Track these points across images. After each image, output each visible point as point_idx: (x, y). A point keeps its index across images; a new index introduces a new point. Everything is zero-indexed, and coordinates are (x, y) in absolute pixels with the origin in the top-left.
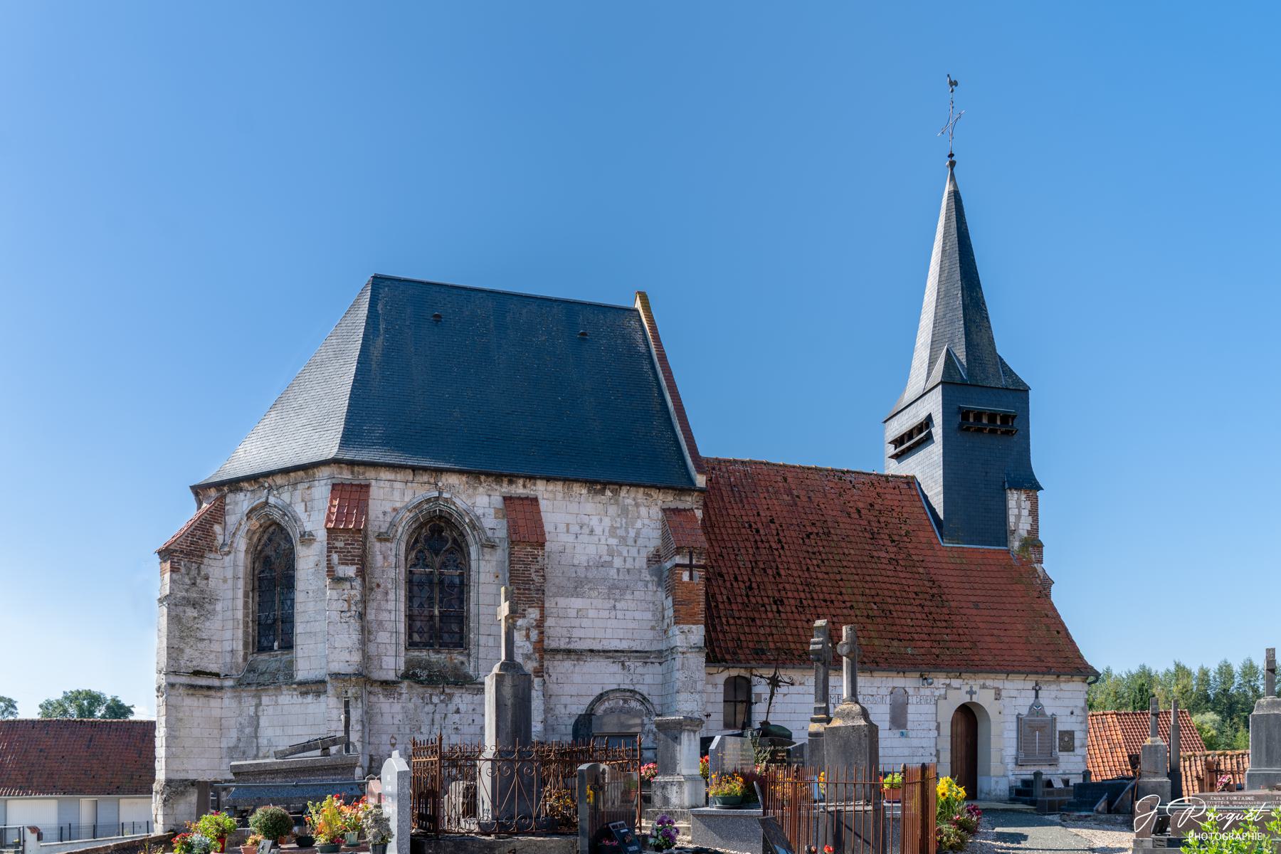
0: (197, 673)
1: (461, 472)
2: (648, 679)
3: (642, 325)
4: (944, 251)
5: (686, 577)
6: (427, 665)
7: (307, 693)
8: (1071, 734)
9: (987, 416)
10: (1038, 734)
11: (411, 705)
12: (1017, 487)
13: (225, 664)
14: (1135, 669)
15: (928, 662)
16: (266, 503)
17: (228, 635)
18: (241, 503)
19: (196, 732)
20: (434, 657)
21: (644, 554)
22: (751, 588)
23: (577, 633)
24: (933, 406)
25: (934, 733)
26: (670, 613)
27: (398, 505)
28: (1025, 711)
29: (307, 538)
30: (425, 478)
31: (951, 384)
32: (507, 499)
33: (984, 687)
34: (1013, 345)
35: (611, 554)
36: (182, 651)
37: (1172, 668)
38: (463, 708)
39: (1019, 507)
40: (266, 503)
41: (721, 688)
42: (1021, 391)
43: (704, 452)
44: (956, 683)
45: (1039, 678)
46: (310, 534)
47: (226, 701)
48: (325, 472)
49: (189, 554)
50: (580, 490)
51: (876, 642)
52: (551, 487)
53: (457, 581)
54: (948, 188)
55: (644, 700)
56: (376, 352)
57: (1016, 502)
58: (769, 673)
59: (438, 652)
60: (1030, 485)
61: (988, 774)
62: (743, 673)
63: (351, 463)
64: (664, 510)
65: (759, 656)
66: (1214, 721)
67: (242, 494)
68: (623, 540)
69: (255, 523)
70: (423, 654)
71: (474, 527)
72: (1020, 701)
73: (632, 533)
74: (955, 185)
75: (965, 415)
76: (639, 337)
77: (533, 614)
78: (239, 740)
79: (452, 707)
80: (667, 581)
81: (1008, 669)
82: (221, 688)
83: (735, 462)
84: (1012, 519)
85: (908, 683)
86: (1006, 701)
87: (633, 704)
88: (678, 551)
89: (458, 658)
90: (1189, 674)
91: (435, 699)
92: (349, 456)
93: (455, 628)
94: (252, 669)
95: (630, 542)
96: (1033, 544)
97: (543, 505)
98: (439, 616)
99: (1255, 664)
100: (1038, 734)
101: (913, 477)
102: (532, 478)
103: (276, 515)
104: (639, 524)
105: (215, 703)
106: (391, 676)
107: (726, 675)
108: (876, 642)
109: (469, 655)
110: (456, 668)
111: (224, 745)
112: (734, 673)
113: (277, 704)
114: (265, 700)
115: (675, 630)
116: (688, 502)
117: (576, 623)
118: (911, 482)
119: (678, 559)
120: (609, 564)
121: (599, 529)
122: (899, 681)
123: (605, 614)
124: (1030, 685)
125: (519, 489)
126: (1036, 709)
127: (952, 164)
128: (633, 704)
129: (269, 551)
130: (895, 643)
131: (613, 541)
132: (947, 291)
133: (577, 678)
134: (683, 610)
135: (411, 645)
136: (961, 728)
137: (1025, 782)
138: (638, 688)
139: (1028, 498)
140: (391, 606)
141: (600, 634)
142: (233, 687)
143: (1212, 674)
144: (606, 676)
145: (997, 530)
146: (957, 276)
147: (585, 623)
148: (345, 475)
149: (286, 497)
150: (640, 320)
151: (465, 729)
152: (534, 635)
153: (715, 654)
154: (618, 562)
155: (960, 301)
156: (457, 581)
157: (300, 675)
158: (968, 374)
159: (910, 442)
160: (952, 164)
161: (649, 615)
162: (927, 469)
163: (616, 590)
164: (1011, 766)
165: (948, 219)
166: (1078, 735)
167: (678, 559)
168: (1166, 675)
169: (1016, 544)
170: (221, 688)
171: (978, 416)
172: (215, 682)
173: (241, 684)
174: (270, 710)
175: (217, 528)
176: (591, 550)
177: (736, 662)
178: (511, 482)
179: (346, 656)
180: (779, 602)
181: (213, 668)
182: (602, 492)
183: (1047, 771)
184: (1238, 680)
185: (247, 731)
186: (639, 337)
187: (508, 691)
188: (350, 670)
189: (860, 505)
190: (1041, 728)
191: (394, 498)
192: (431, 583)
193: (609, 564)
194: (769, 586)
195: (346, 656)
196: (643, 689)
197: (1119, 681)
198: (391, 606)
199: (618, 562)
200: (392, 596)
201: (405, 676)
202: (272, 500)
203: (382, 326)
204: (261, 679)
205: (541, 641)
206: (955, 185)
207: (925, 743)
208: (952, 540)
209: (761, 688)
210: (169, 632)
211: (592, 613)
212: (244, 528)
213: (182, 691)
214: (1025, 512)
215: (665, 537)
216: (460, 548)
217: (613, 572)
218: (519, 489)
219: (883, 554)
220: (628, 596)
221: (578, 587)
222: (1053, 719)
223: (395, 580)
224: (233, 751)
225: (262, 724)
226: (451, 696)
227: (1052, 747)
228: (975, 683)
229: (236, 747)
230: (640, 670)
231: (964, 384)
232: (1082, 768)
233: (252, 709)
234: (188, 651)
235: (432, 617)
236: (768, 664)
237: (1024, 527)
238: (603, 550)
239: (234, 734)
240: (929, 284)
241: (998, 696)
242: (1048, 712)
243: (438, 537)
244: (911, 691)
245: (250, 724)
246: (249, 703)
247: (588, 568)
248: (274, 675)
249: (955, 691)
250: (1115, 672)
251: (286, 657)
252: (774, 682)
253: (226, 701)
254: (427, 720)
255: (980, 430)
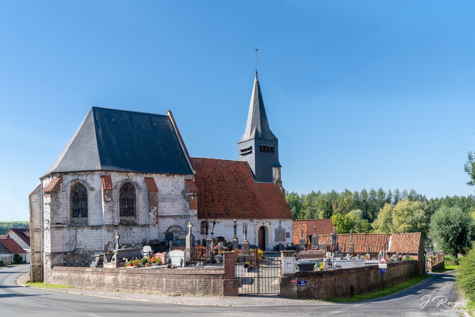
0: (57, 224)
1: (134, 172)
2: (182, 223)
3: (171, 122)
4: (254, 99)
5: (193, 198)
6: (125, 221)
7: (93, 229)
8: (289, 233)
9: (266, 146)
10: (280, 233)
11: (122, 231)
12: (275, 166)
13: (64, 221)
14: (330, 191)
15: (252, 217)
16: (78, 179)
17: (65, 213)
18: (68, 179)
19: (58, 239)
20: (127, 219)
21: (180, 191)
22: (205, 197)
23: (164, 212)
24: (252, 144)
25: (254, 234)
26: (188, 206)
27: (118, 181)
28: (277, 228)
29: (92, 189)
30: (124, 174)
31: (257, 138)
32: (146, 178)
33: (266, 222)
34: (275, 127)
35: (172, 191)
36: (54, 218)
37: (344, 191)
38: (135, 231)
39: (276, 172)
40: (78, 179)
41: (200, 224)
42: (276, 141)
43: (191, 156)
44: (259, 221)
45: (281, 219)
46: (93, 188)
47: (65, 231)
48: (98, 172)
49: (55, 192)
50: (164, 175)
51: (239, 211)
52: (156, 175)
53: (132, 199)
54: (255, 80)
55: (181, 228)
56: (100, 134)
57: (275, 170)
58: (213, 220)
59: (127, 217)
60: (279, 166)
61: (268, 244)
62: (205, 220)
63: (106, 171)
64: (185, 180)
65: (210, 216)
66: (359, 213)
67: (68, 176)
68: (175, 188)
69: (73, 183)
70: (124, 218)
71: (137, 186)
72: (276, 225)
73: (177, 186)
74: (258, 80)
75: (261, 148)
76: (171, 125)
77: (155, 208)
78: (70, 241)
79: (132, 231)
80: (188, 199)
81: (273, 218)
82: (63, 227)
83: (197, 158)
84: (274, 175)
85: (247, 221)
86: (272, 225)
87: (178, 229)
88: (191, 192)
89: (133, 218)
90: (350, 194)
91: (128, 230)
92: (105, 168)
93: (131, 211)
94: (72, 222)
95: (177, 188)
96: (279, 181)
97: (155, 179)
98: (127, 207)
99: (375, 190)
100: (280, 233)
101: (247, 162)
102: (152, 173)
103: (81, 182)
104: (179, 184)
105: (62, 231)
106: (117, 224)
107: (201, 221)
108: (239, 211)
109: (136, 218)
110: (133, 221)
111: (64, 242)
112: (203, 220)
113: (83, 231)
114: (79, 230)
115: (190, 211)
116: (191, 177)
117: (164, 209)
118: (246, 163)
119: (191, 194)
120: (172, 194)
121: (170, 186)
122: (245, 221)
123: (171, 207)
124: (278, 221)
125: (148, 176)
126: (280, 227)
127: (257, 73)
128: (178, 229)
129: (77, 190)
130: (244, 211)
131: (172, 188)
132: (256, 111)
133: (164, 223)
134: (192, 206)
135: (121, 215)
136: (261, 232)
137: (277, 246)
138: (179, 225)
139: (278, 169)
140: (116, 206)
141: (170, 212)
142: (67, 227)
143: (359, 194)
144: (171, 222)
145: (270, 178)
146: (258, 107)
147: (166, 209)
148: (104, 173)
149: (84, 178)
150: (170, 120)
151: (136, 237)
152: (156, 213)
153: (200, 216)
154: (174, 193)
155: (259, 115)
156: (132, 199)
157: (91, 224)
158: (262, 136)
159: (246, 152)
160: (257, 73)
161: (182, 207)
162: (251, 159)
163: (173, 200)
164: (274, 242)
165: (256, 89)
166: (290, 233)
167: (191, 194)
168: (342, 194)
169: (275, 182)
170: (63, 227)
171: (265, 147)
172: (61, 226)
173: (69, 226)
174: (81, 233)
175: (61, 184)
176: (167, 190)
177: (204, 218)
178: (146, 174)
179: (109, 220)
180: (213, 200)
181: (61, 222)
182: (169, 176)
183: (282, 243)
184: (369, 196)
185: (73, 239)
186: (171, 125)
187: (191, 239)
188: (110, 224)
189: (233, 171)
190: (281, 232)
191: (117, 178)
192: (125, 199)
193: (172, 194)
194: (210, 196)
195: (109, 220)
196: (181, 225)
197: (324, 196)
198: (116, 206)
199: (174, 193)
200: (116, 204)
201: (120, 224)
202: (80, 178)
203: (99, 125)
204: (77, 225)
205: (157, 215)
206: (258, 80)
207: (252, 236)
208: (258, 181)
209: (211, 225)
210: (51, 213)
211: (167, 206)
212: (70, 185)
213: (54, 229)
214: (277, 173)
215: (185, 187)
216: (133, 189)
217: (173, 196)
218: (148, 176)
219: (239, 186)
220: (176, 202)
221: (164, 200)
222: (284, 230)
223: (117, 200)
224: (67, 244)
225: (78, 236)
226: (132, 229)
227: (284, 237)
228: (264, 221)
229: (69, 243)
230: (180, 220)
231: (260, 139)
232: (292, 242)
233: (74, 233)
234: (55, 218)
235: (125, 208)
236: (212, 218)
237: (277, 177)
238: (170, 190)
239: (68, 239)
240: (250, 106)
241: (270, 224)
242: (283, 228)
243: (128, 189)
244: (248, 223)
245: (73, 237)
246: (73, 231)
247: (166, 195)
248: (81, 224)
249: (259, 223)
250: (322, 192)
251: (85, 219)
252: (214, 223)
253: (65, 231)
254: (126, 235)
255: (265, 151)
